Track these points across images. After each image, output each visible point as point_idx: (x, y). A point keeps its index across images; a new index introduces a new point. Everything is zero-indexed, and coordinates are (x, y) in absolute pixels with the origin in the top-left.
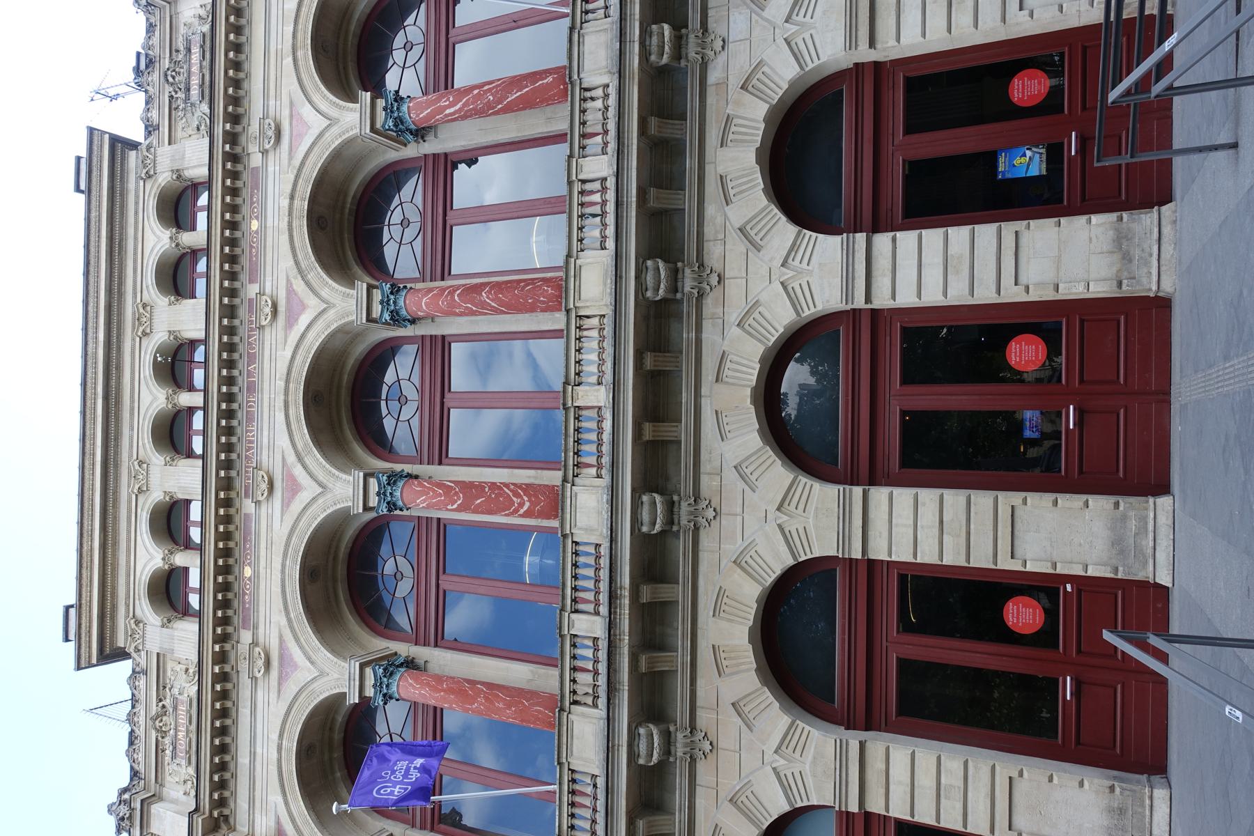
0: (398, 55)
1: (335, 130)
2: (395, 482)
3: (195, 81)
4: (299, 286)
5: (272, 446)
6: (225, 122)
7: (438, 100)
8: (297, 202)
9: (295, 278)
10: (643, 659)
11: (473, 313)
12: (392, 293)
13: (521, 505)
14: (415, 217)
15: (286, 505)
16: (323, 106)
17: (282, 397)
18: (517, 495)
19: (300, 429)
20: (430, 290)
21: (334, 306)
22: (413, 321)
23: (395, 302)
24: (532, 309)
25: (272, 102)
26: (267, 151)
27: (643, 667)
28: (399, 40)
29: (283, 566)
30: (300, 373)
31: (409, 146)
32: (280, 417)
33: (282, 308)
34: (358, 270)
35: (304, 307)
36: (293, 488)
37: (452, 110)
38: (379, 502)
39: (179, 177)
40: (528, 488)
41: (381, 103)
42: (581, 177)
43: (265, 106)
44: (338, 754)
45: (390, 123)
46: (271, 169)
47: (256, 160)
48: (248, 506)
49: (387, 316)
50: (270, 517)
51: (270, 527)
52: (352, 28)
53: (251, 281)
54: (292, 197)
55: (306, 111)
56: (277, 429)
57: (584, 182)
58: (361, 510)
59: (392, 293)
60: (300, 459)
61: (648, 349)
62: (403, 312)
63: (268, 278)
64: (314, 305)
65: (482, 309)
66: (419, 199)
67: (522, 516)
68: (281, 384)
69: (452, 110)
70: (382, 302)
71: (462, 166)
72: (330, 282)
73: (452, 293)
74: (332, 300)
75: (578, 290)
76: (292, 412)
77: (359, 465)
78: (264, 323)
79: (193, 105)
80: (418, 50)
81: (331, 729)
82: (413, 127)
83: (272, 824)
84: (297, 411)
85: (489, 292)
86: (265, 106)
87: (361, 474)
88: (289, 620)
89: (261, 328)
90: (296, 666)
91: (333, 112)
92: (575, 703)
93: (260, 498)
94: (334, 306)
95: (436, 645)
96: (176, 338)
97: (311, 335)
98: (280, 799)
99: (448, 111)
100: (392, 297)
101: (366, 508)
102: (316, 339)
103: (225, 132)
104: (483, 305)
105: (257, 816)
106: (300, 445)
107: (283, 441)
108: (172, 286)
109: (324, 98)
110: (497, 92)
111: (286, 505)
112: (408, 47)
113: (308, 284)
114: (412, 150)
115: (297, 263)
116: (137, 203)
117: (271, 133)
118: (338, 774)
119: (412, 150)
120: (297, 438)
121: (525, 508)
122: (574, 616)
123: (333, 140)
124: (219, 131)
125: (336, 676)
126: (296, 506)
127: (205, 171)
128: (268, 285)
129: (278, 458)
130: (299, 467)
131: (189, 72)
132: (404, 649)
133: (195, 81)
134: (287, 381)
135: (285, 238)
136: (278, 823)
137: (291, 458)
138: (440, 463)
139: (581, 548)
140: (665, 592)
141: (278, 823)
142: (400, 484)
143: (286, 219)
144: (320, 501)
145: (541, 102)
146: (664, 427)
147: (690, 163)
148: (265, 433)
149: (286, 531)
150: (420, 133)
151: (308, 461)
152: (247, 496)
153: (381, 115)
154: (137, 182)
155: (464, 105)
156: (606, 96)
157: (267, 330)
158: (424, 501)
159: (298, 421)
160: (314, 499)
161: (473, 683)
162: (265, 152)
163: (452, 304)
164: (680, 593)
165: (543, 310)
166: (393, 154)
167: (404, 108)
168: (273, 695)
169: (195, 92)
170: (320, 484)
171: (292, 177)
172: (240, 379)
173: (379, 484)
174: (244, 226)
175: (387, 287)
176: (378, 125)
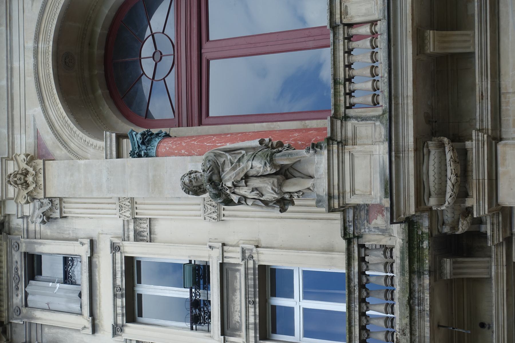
2: (149, 141)
10: (448, 265)
12: (143, 143)
14: (166, 48)
27: (431, 48)
34: (108, 110)
42: (345, 21)
44: (98, 71)
52: (99, 30)
57: (350, 25)
59: (143, 143)
61: (432, 27)
66: (171, 31)
77: (111, 129)
80: (168, 61)
81: (91, 45)
83: (31, 140)
87: (114, 135)
98: (38, 110)
100: (144, 147)
105: (17, 136)
118: (100, 92)
136: (37, 137)
138: (200, 124)
139: (354, 31)
140: (456, 42)
141: (37, 137)
146: (456, 35)
147: (482, 84)
156: (374, 34)
164: (477, 41)
173: (133, 145)
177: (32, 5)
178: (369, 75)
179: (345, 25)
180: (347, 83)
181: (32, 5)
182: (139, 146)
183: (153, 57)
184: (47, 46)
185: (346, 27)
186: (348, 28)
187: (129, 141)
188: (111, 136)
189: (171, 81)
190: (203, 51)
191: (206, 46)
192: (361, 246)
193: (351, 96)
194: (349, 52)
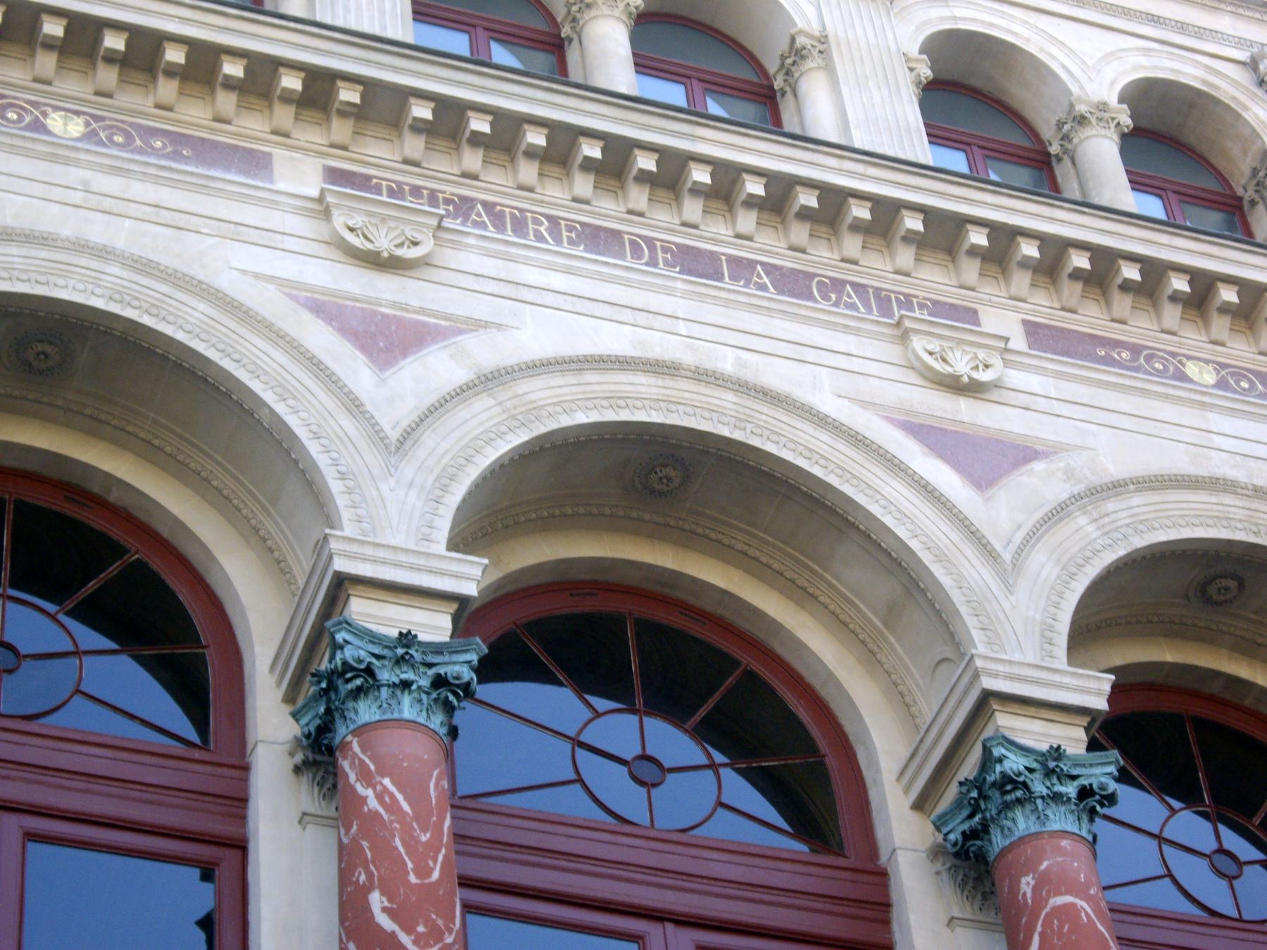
0: (621, 730)
4: (1040, 485)
5: (514, 293)
15: (325, 308)
17: (687, 358)
23: (1057, 798)
26: (326, 213)
28: (672, 742)
29: (104, 253)
31: (915, 817)
32: (615, 339)
33: (964, 410)
35: (983, 481)
38: (374, 638)
41: (1073, 739)
45: (355, 652)
48: (299, 174)
50: (266, 238)
51: (235, 232)
53: (1033, 330)
58: (340, 565)
60: (489, 381)
62: (366, 711)
68: (727, 362)
71: (203, 898)
76: (643, 384)
78: (919, 344)
80: (1216, 894)
82: (998, 841)
84: (647, 402)
89: (904, 337)
94: (1009, 588)
96: (797, 54)
97: (896, 490)
100: (1070, 789)
102: (889, 504)
107: (536, 336)
108: (948, 77)
111: (325, 308)
112: (647, 771)
113: (1059, 513)
114: (272, 725)
115: (1117, 487)
116: (1182, 27)
119: (272, 725)
123: (956, 572)
126: (321, 338)
129: (481, 308)
130: (460, 375)
134: (743, 387)
135: (1178, 461)
137: (486, 352)
142: (437, 721)
143: (1240, 475)
144: (348, 424)
149: (226, 282)
150: (319, 755)
152: (335, 176)
153: (1036, 733)
154: (1240, 43)
157: (892, 351)
158: (393, 807)
159: (613, 400)
160: (354, 405)
166: (264, 626)
170: (409, 436)
173: (438, 649)
174: (73, 85)
175: (461, 668)
176: (1006, 721)
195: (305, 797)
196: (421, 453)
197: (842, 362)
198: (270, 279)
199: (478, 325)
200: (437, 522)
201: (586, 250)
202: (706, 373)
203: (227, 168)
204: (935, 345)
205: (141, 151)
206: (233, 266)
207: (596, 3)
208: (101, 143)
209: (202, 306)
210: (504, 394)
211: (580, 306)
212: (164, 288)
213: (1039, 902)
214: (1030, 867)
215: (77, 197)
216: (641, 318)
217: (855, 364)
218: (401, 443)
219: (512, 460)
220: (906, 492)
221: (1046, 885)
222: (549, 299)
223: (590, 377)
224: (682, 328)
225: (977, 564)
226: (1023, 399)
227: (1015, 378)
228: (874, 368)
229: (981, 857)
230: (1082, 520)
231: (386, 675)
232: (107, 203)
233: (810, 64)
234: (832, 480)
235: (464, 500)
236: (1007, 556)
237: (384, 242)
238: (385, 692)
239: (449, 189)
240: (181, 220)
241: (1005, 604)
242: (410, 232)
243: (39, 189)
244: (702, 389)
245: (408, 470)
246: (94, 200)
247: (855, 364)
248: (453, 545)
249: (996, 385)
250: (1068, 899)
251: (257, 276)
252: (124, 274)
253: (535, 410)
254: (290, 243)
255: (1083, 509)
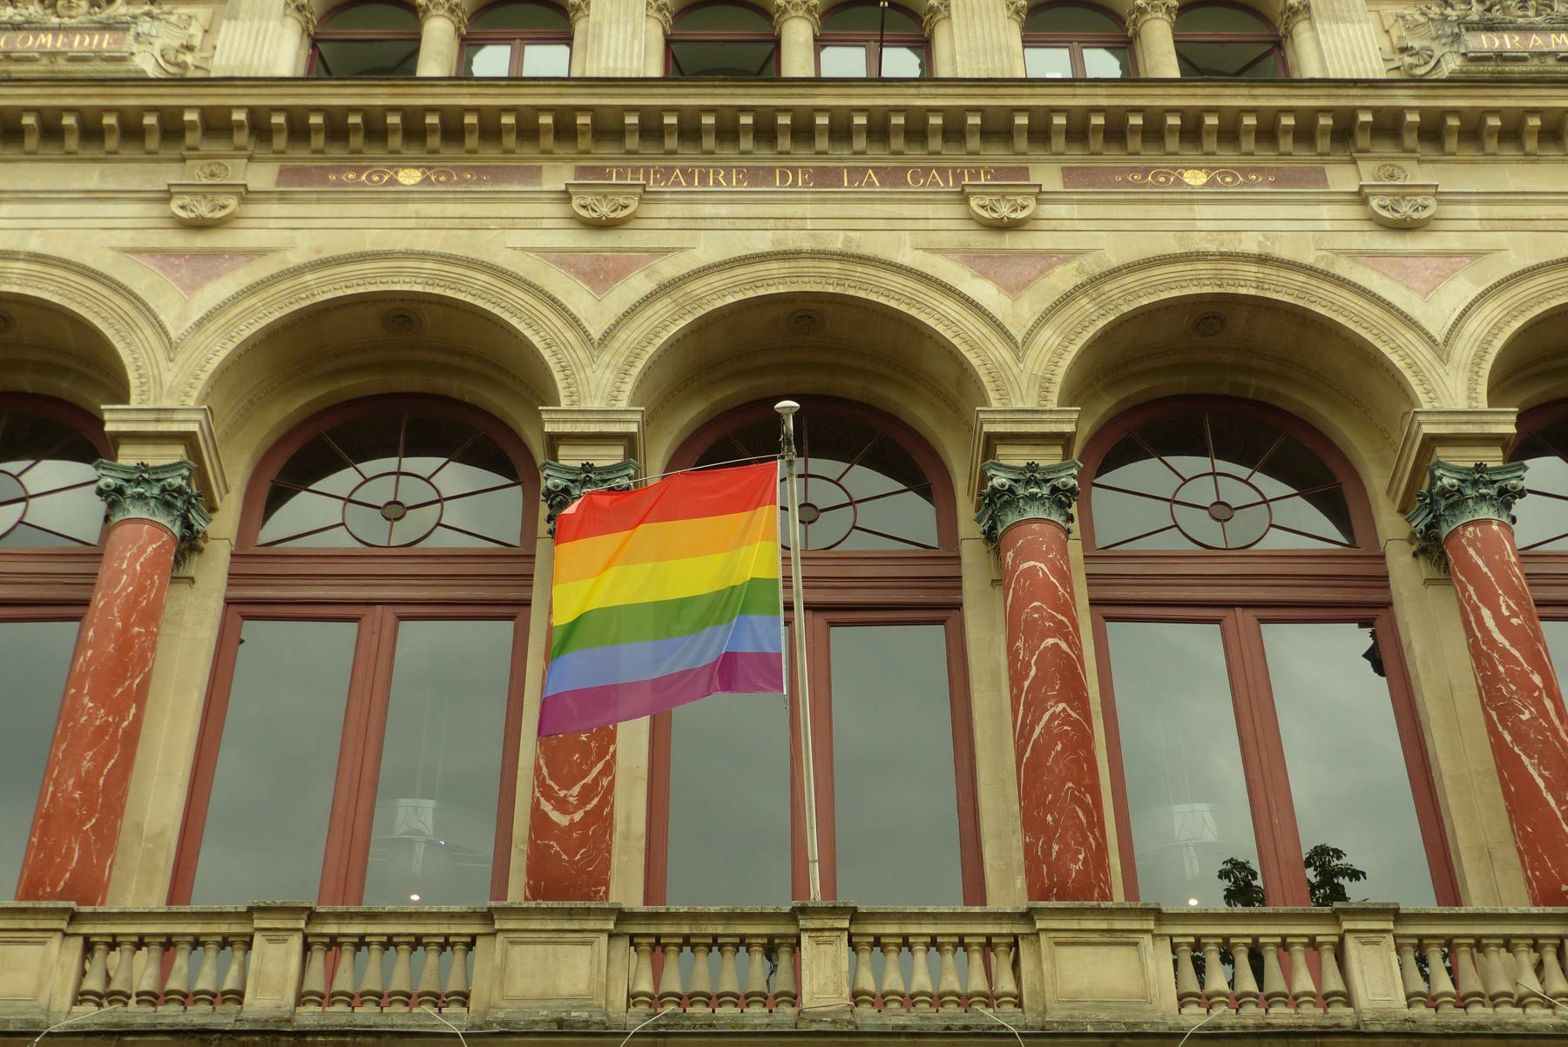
1: (1424, 354)
3: (1508, 42)
4: (1064, 278)
5: (694, 224)
6: (1422, 111)
7: (1512, 591)
8: (1252, 270)
9: (1080, 270)
11: (1016, 679)
12: (1055, 490)
13: (562, 806)
14: (1241, 530)
16: (1476, 326)
17: (807, 246)
18: (585, 796)
19: (735, 287)
20: (1066, 579)
21: (1019, 359)
22: (990, 536)
24: (1031, 822)
25: (1475, 211)
29: (423, 256)
30: (862, 284)
32: (762, 242)
35: (1013, 290)
36: (599, 275)
37: (1490, 623)
38: (569, 470)
39: (1294, 12)
40: (601, 821)
42: (1350, 942)
43: (1465, 198)
46: (1325, 211)
47: (1342, 178)
49: (1000, 480)
50: (533, 224)
51: (512, 223)
53: (1067, 173)
54: (1263, 260)
55: (1462, 289)
56: (726, 236)
59: (1055, 490)
62: (1011, 518)
63: (1075, 211)
64: (1018, 312)
65: (1027, 705)
66: (1277, 541)
67: (536, 809)
68: (837, 243)
69: (1490, 623)
70: (1032, 467)
71: (1362, 639)
72: (1074, 349)
73: (1060, 630)
74: (1032, 353)
75: (1078, 940)
76: (774, 268)
77: (650, 420)
78: (974, 203)
79: (1457, 37)
80: (1211, 533)
82: (1445, 531)
84: (777, 281)
85: (1067, 720)
86: (1465, 198)
87: (633, 428)
88: (298, 271)
90: (191, 287)
91: (1464, 349)
92: (89, 947)
93: (576, 202)
94: (1019, 359)
95: (229, 602)
97: (950, 307)
99: (1486, 613)
100: (1046, 491)
101: (554, 441)
102: (942, 318)
103: (1399, 113)
104: (1035, 706)
106: (698, 287)
107: (707, 248)
109: (1493, 329)
110: (1540, 730)
111: (561, 258)
113: (1067, 298)
115: (1114, 273)
117: (1406, 210)
119: (1392, 528)
120: (716, 280)
121: (555, 816)
122: (296, 942)
123: (1399, 350)
124: (1401, 99)
125: (168, 378)
126: (559, 283)
127: (1311, 70)
128: (1062, 210)
129: (670, 240)
131: (1530, 29)
132: (223, 526)
133: (1508, 42)
134: (843, 257)
135: (1171, 245)
137: (669, 268)
138: (1094, 603)
143: (1212, 248)
145: (1525, 838)
148: (724, 210)
149: (501, 259)
150: (1432, 547)
151: (662, 307)
155: (1503, 652)
159: (753, 283)
160: (574, 322)
161: (141, 696)
162: (1361, 197)
163: (1034, 632)
165: (1028, 850)
167: (1486, 512)
168: (127, 239)
169: (1485, 42)
170: (609, 335)
171: (1309, 258)
172: (846, 153)
173: (610, 470)
175: (1068, 479)
177: (112, 249)
178: (692, 989)
179: (1342, 939)
180: (1472, 941)
181: (112, 249)
182: (159, 480)
183: (1219, 503)
184: (1246, 282)
185: (1336, 939)
186: (1332, 943)
187: (1057, 461)
188: (1070, 421)
189: (1172, 542)
190: (1239, 610)
191: (1249, 616)
192: (470, 945)
193: (955, 946)
194: (961, 942)
195: (1424, 569)
196: (616, 345)
197: (921, 225)
198: (531, 250)
199: (666, 251)
200: (624, 387)
201: (750, 185)
202: (819, 252)
203: (511, 182)
204: (1387, 201)
205: (457, 183)
206: (503, 247)
207: (1307, 8)
208: (432, 184)
209: (484, 277)
210: (678, 294)
211: (739, 224)
212: (460, 270)
213: (1015, 566)
214: (1012, 546)
215: (411, 223)
216: (780, 224)
217: (931, 224)
218: (1024, 343)
219: (685, 336)
220: (955, 307)
221: (1022, 555)
222: (718, 224)
223: (738, 271)
224: (809, 224)
225: (999, 345)
226: (1053, 224)
227: (1048, 210)
228: (944, 224)
229: (1437, 539)
230: (1084, 301)
231: (1021, 491)
232: (430, 223)
233: (940, 16)
234: (903, 308)
235: (126, 375)
236: (1019, 339)
237: (604, 210)
238: (1021, 503)
239: (658, 164)
240: (476, 223)
241: (1015, 370)
242: (622, 201)
243: (386, 223)
244: (817, 264)
245: (606, 357)
246: (422, 222)
247: (931, 224)
248: (1492, 400)
249: (1033, 218)
250: (1032, 563)
251: (523, 249)
252: (436, 266)
253: (699, 300)
254: (547, 223)
255: (1086, 294)
